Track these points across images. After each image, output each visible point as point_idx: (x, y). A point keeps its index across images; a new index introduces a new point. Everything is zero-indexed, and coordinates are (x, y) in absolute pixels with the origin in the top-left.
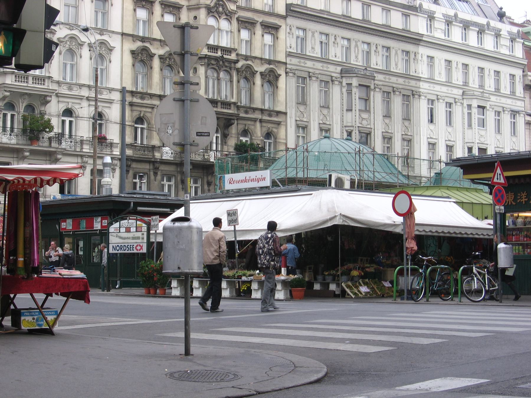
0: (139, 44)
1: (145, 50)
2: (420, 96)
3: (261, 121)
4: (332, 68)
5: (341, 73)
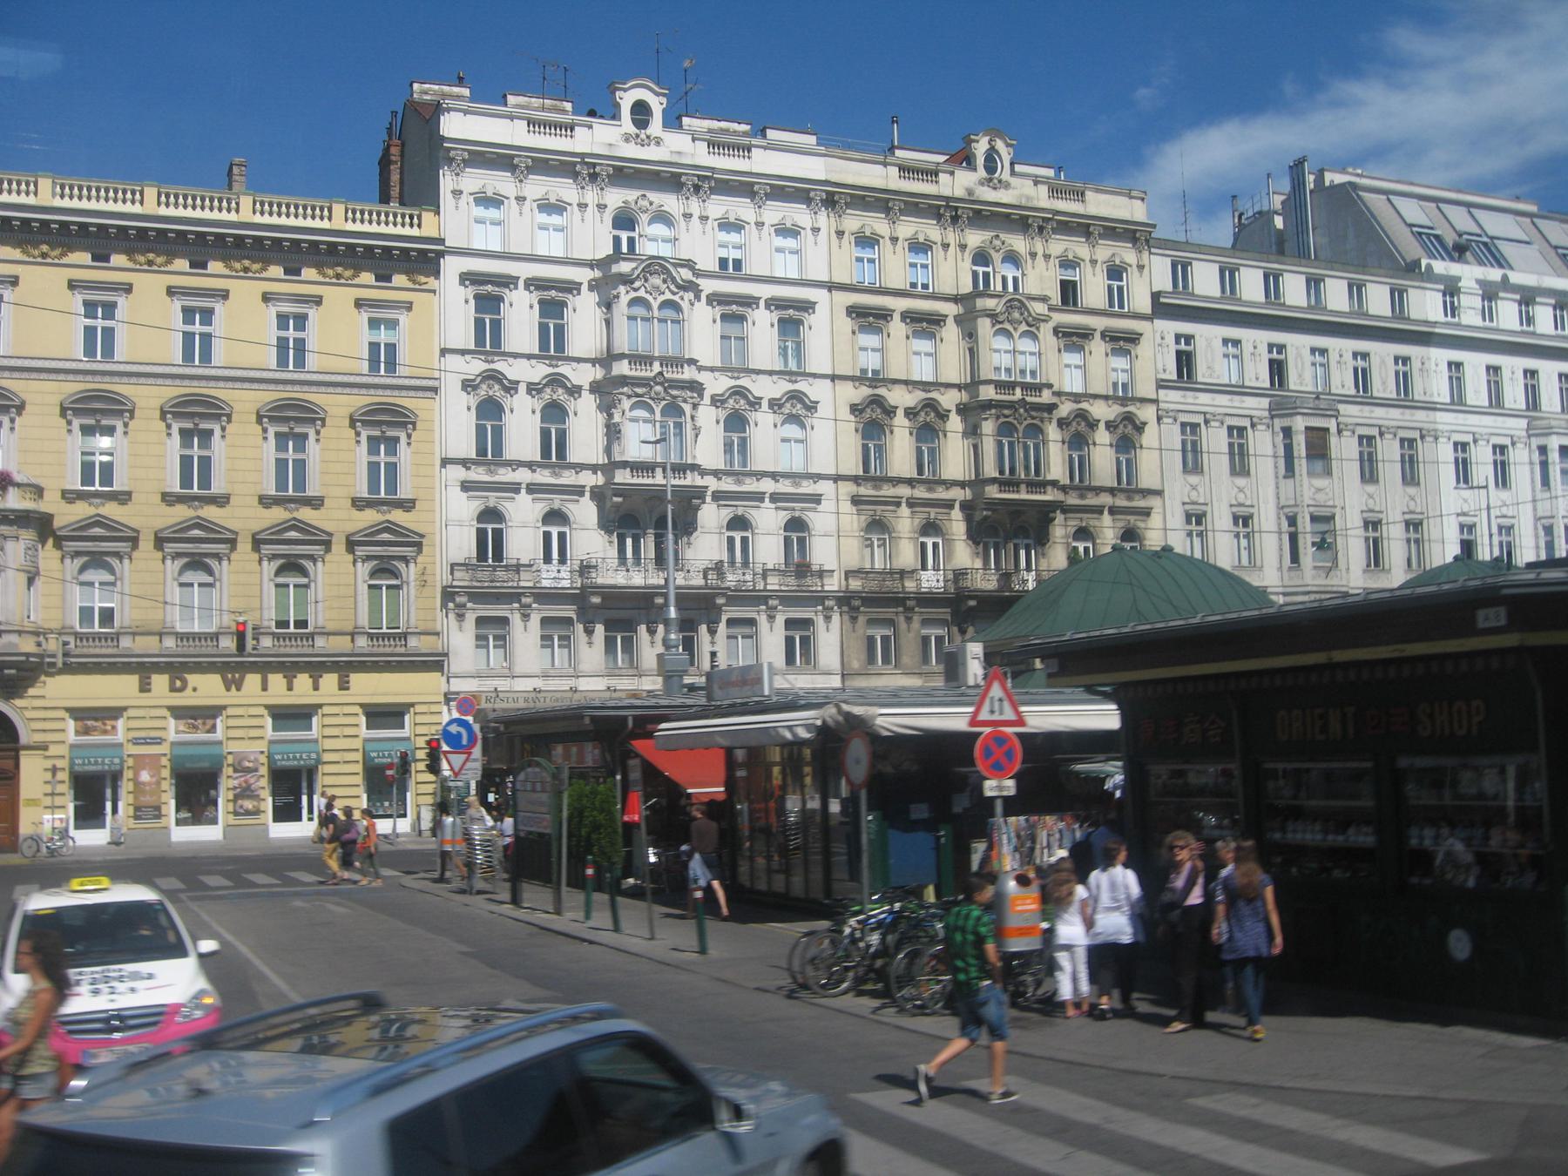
0: (865, 391)
1: (877, 401)
2: (1436, 438)
3: (912, 503)
4: (1250, 402)
5: (1270, 410)
